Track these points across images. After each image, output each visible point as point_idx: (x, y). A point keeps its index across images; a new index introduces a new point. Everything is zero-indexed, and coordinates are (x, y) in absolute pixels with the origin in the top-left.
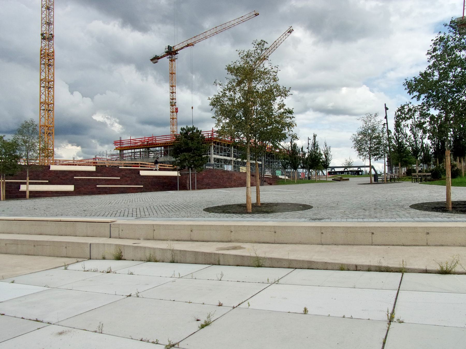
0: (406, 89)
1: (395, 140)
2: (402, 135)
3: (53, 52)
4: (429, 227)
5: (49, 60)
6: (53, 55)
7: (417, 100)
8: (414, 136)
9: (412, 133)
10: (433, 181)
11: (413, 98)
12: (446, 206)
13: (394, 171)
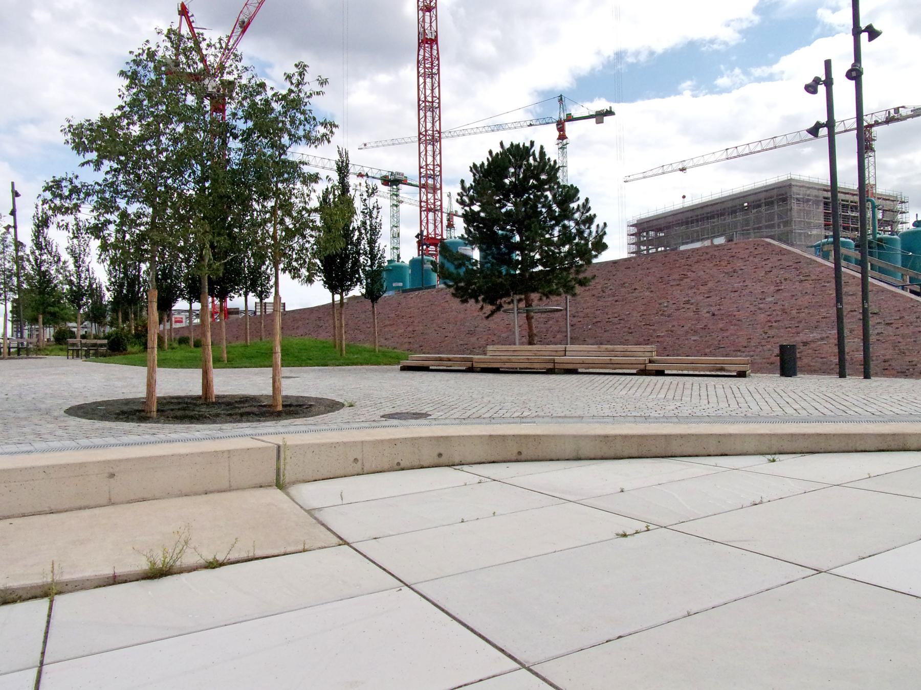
0: (68, 142)
1: (33, 265)
2: (49, 256)
4: (115, 461)
7: (95, 170)
8: (76, 261)
9: (72, 255)
10: (110, 355)
11: (83, 164)
12: (146, 408)
13: (26, 333)
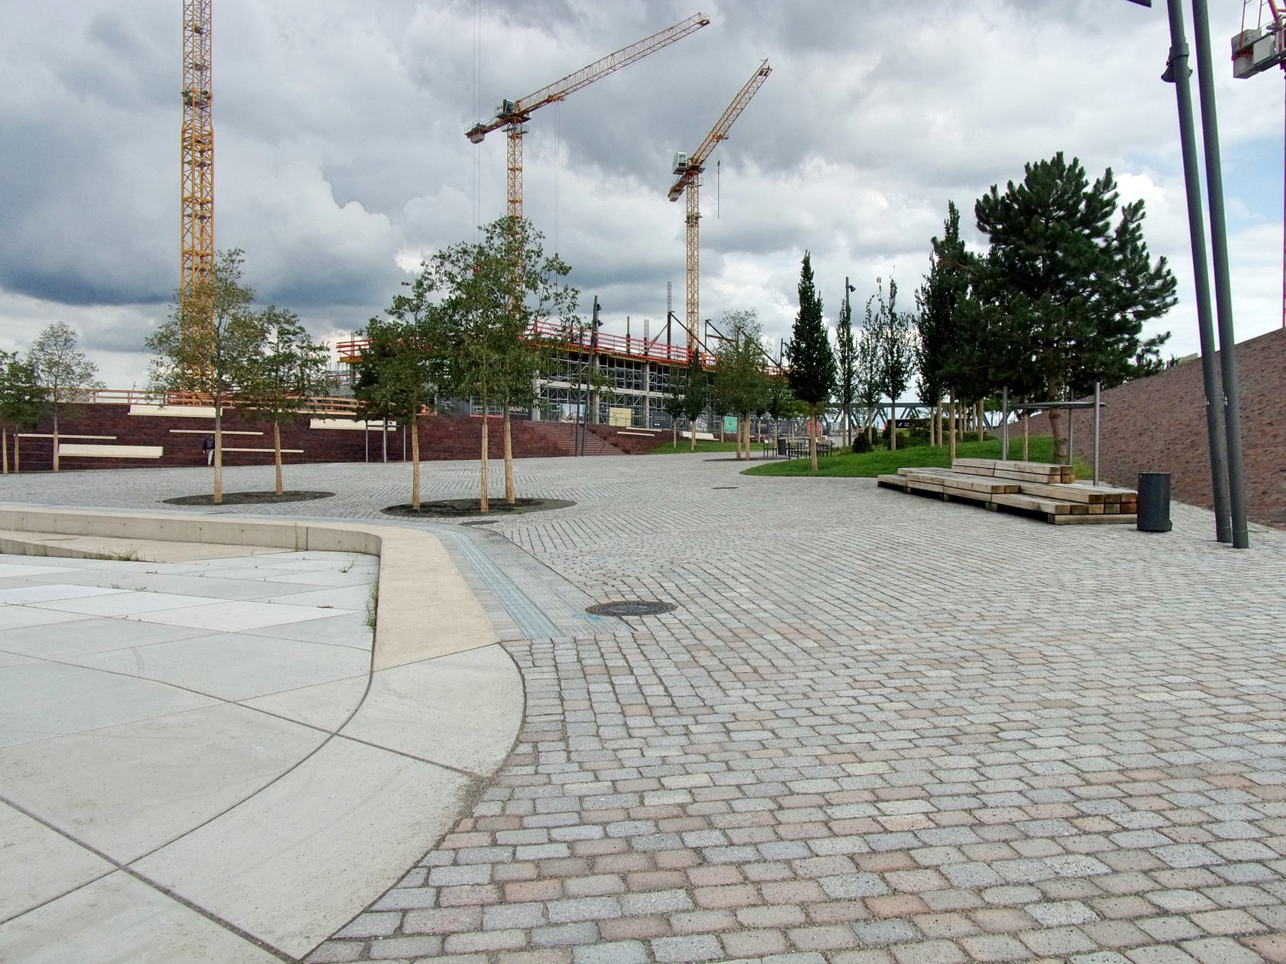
3: (210, 134)
5: (202, 152)
6: (211, 142)
